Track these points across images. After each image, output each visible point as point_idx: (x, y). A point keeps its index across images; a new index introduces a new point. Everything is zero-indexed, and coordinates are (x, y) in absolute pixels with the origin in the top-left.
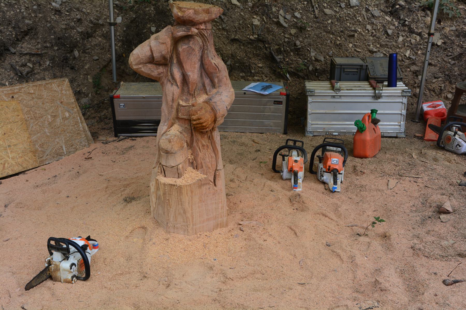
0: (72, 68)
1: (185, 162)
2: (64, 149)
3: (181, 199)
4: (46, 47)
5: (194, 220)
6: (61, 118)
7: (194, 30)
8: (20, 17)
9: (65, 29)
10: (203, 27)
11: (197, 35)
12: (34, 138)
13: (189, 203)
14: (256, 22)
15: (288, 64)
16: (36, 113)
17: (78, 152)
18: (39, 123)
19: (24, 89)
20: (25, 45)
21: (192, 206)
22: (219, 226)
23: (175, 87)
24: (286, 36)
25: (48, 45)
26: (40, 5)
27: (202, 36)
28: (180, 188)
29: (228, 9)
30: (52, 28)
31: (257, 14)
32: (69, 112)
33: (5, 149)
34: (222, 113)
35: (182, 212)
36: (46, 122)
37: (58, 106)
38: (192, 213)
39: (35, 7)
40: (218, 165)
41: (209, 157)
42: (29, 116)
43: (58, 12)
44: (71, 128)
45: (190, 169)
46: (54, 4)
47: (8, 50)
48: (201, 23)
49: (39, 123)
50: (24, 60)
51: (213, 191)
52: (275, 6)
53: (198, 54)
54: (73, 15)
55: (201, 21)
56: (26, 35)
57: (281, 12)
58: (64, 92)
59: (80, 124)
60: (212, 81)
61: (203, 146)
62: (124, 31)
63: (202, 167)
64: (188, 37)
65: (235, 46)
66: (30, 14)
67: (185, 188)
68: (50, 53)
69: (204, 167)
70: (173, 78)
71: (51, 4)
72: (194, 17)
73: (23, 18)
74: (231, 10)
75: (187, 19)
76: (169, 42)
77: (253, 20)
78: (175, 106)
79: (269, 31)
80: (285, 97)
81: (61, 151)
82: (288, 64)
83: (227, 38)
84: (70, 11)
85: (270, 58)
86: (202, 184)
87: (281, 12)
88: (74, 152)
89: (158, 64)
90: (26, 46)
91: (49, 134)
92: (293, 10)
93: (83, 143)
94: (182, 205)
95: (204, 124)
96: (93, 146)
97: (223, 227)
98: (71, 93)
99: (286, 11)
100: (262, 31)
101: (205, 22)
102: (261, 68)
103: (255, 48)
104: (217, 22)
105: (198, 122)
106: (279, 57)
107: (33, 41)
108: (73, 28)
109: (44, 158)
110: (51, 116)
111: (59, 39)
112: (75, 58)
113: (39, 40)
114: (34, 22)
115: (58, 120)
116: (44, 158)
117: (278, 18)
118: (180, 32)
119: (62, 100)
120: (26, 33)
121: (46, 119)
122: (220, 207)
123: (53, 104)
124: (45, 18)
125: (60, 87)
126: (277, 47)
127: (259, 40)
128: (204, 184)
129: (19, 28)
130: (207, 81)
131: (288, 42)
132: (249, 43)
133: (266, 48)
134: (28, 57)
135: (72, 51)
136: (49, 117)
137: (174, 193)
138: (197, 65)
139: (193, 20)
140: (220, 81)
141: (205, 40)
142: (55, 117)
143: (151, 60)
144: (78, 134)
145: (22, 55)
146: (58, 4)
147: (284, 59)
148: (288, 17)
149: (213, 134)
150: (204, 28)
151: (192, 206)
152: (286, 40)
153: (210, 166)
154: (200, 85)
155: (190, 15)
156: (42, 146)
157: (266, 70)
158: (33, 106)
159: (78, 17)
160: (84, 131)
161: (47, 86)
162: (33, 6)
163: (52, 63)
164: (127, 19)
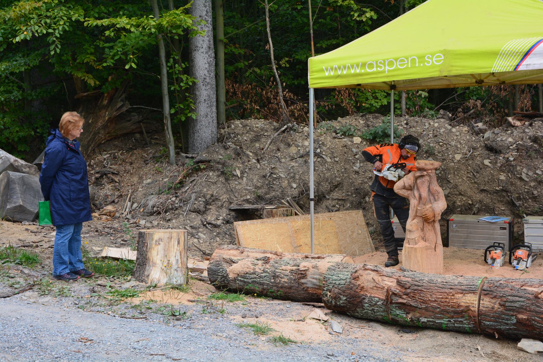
0: (364, 209)
1: (419, 237)
4: (348, 195)
7: (425, 173)
8: (334, 176)
9: (361, 183)
10: (430, 171)
11: (426, 175)
12: (341, 243)
14: (502, 177)
15: (526, 208)
20: (335, 194)
23: (415, 200)
24: (526, 187)
25: (349, 194)
27: (429, 176)
28: (416, 249)
29: (481, 169)
30: (352, 183)
31: (503, 172)
33: (325, 247)
34: (438, 212)
39: (343, 170)
43: (357, 173)
46: (355, 168)
47: (325, 197)
50: (334, 203)
52: (520, 166)
53: (427, 184)
54: (367, 174)
56: (336, 188)
57: (525, 170)
60: (434, 198)
64: (422, 176)
65: (483, 194)
66: (339, 174)
68: (351, 198)
70: (415, 196)
73: (336, 177)
74: (483, 169)
76: (412, 178)
77: (500, 176)
78: (415, 210)
79: (512, 184)
80: (508, 225)
82: (526, 208)
83: (478, 189)
84: (365, 171)
85: (511, 204)
87: (525, 170)
88: (363, 255)
89: (408, 189)
90: (336, 195)
92: (535, 168)
93: (369, 250)
96: (375, 253)
99: (529, 169)
100: (506, 184)
101: (431, 170)
102: (504, 210)
103: (500, 196)
106: (519, 202)
107: (340, 191)
108: (366, 183)
111: (357, 189)
112: (366, 202)
113: (344, 191)
114: (342, 179)
115: (355, 234)
117: (521, 174)
118: (418, 174)
120: (336, 186)
124: (348, 176)
126: (517, 195)
127: (502, 190)
129: (333, 183)
130: (432, 198)
131: (528, 192)
132: (495, 193)
133: (508, 196)
134: (336, 201)
135: (364, 198)
138: (427, 190)
140: (439, 198)
142: (353, 232)
143: (404, 188)
145: (333, 199)
147: (523, 205)
148: (530, 173)
152: (526, 190)
154: (428, 200)
156: (344, 248)
157: (507, 212)
159: (370, 175)
160: (370, 243)
163: (351, 205)
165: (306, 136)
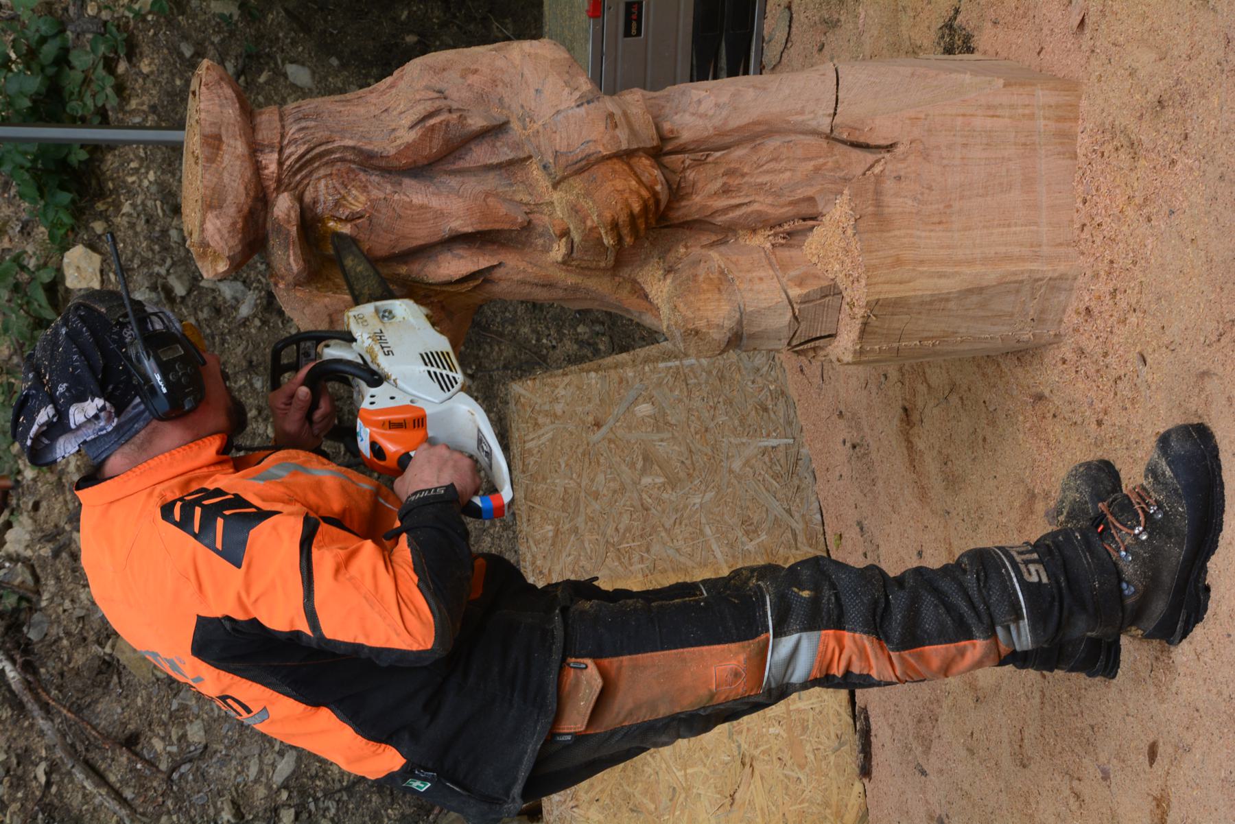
2: (774, 442)
3: (922, 303)
5: (1016, 250)
6: (656, 437)
10: (270, 162)
13: (942, 275)
16: (628, 529)
17: (792, 392)
18: (668, 523)
19: (540, 556)
21: (959, 263)
22: (1066, 125)
26: (251, 362)
32: (635, 402)
35: (975, 299)
36: (665, 496)
37: (610, 441)
38: (985, 260)
40: (813, 124)
41: (772, 171)
42: (636, 558)
44: (697, 403)
45: (814, 242)
48: (258, 168)
49: (668, 523)
51: (912, 158)
55: (248, 174)
58: (559, 408)
59: (687, 362)
61: (726, 191)
62: (344, 66)
63: (811, 200)
67: (878, 288)
69: (810, 192)
71: (247, 319)
72: (232, 211)
75: (241, 241)
81: (781, 455)
86: (875, 215)
88: (791, 404)
91: (710, 495)
94: (947, 300)
95: (636, 208)
97: (1075, 107)
98: (567, 379)
101: (255, 149)
104: (254, 83)
105: (625, 231)
109: (799, 527)
110: (644, 471)
116: (799, 527)
119: (590, 419)
121: (655, 492)
122: (989, 123)
123: (602, 460)
125: (540, 421)
128: (878, 204)
130: (480, 154)
136: (646, 480)
137: (896, 325)
139: (246, 209)
141: (320, 156)
144: (721, 378)
146: (244, 294)
149: (686, 136)
150: (275, 156)
151: (959, 263)
153: (810, 165)
154: (492, 181)
155: (225, 231)
158: (604, 534)
161: (532, 468)
162: (254, 390)
164: (294, 43)
165: (56, 554)
